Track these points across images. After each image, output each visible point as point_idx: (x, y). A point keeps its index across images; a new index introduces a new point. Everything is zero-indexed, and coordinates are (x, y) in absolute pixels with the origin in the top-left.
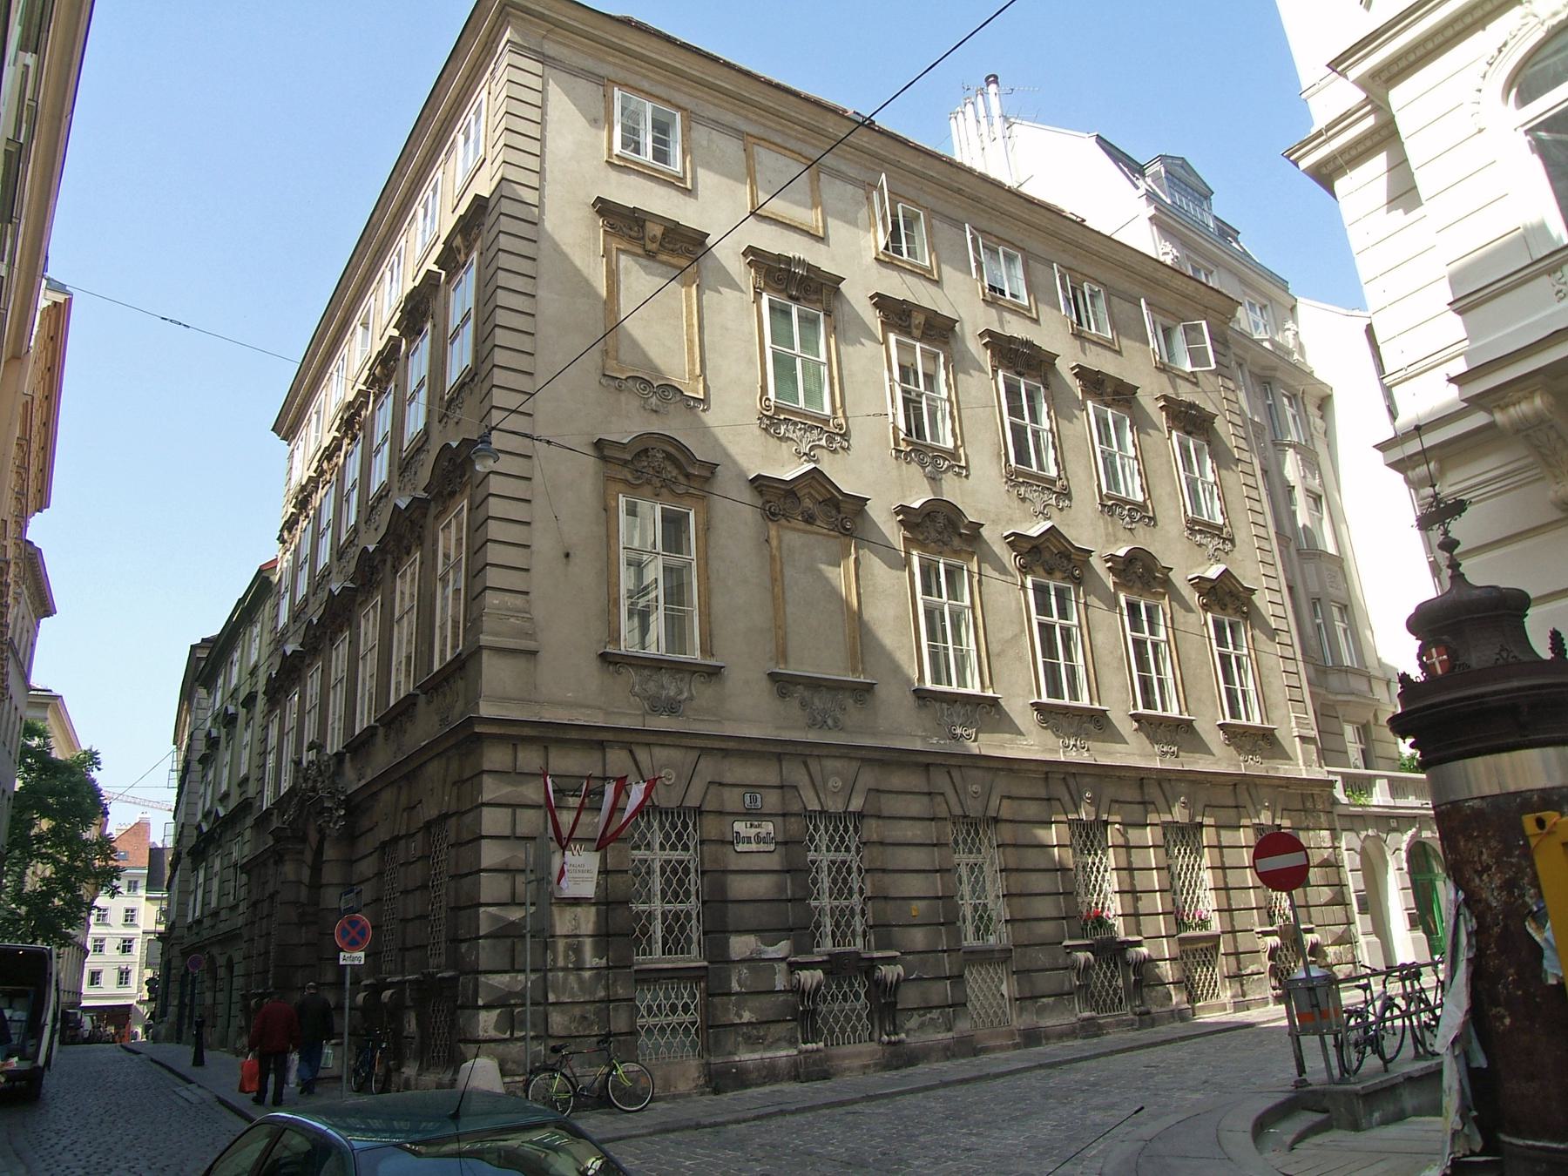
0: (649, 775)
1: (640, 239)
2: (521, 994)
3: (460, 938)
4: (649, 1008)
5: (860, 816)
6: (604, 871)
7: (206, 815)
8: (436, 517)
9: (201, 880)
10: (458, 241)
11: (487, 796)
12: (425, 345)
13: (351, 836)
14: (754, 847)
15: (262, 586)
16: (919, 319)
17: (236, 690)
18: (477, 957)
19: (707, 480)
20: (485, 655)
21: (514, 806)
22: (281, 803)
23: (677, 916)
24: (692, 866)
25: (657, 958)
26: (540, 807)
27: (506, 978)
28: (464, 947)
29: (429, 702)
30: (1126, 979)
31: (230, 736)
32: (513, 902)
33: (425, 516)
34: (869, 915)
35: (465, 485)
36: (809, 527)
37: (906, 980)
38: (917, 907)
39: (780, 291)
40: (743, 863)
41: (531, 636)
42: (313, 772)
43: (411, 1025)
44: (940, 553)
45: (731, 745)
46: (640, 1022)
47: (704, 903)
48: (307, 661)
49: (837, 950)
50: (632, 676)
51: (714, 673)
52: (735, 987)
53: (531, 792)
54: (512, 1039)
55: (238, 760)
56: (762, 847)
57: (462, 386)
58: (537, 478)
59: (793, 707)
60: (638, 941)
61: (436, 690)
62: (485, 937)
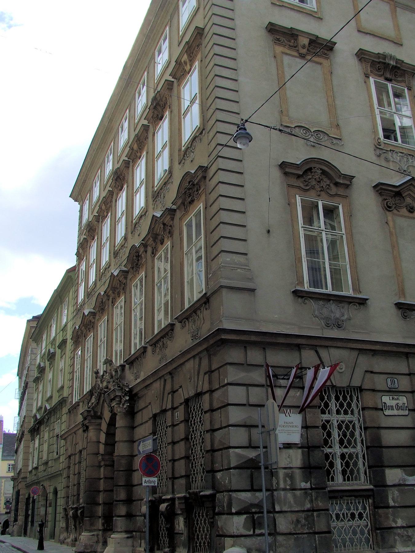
2: (259, 506)
6: (305, 427)
7: (39, 409)
8: (181, 219)
9: (37, 445)
10: (103, 207)
12: (165, 124)
14: (395, 412)
15: (70, 279)
17: (54, 339)
25: (339, 482)
26: (263, 386)
27: (249, 494)
29: (183, 327)
33: (173, 219)
35: (200, 195)
39: (380, 76)
41: (251, 280)
42: (107, 377)
43: (180, 524)
45: (377, 347)
46: (333, 525)
47: (367, 448)
50: (313, 305)
51: (363, 302)
52: (391, 503)
55: (56, 378)
56: (401, 412)
57: (194, 139)
58: (247, 186)
60: (328, 472)
61: (187, 319)
62: (234, 468)
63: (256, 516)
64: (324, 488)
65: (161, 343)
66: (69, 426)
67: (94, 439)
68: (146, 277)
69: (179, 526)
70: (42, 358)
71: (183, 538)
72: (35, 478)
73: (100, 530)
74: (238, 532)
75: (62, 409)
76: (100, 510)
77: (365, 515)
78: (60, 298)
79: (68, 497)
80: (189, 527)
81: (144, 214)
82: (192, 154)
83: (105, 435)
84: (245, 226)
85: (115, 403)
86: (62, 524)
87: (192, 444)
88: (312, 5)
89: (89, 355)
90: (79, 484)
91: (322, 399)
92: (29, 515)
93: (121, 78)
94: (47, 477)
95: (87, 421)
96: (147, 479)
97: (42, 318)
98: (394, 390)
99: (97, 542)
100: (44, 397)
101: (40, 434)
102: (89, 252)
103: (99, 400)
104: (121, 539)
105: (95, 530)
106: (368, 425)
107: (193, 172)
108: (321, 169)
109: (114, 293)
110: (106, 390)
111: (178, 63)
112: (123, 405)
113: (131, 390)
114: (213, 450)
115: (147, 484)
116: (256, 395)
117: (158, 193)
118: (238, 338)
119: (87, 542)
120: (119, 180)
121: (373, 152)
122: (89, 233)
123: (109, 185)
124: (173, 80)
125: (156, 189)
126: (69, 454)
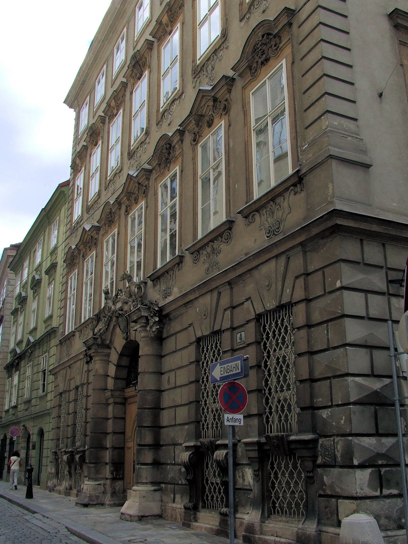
8: (103, 235)
9: (16, 381)
10: (113, 104)
15: (62, 195)
17: (40, 265)
24: (293, 403)
26: (382, 294)
29: (154, 286)
61: (257, 211)
62: (355, 403)
63: (383, 470)
65: (209, 249)
66: (60, 359)
67: (101, 372)
68: (118, 234)
69: (244, 480)
70: (24, 287)
71: (251, 496)
72: (14, 418)
73: (107, 479)
74: (362, 492)
75: (50, 341)
76: (107, 456)
78: (48, 218)
79: (59, 439)
80: (263, 482)
81: (119, 172)
82: (170, 116)
83: (115, 367)
84: (352, 84)
85: (139, 326)
86: (49, 469)
87: (266, 373)
89: (88, 278)
90: (75, 425)
92: (5, 457)
93: (100, 27)
94: (30, 417)
95: (91, 352)
96: (230, 416)
97: (22, 248)
98: (42, 413)
99: (104, 493)
100: (25, 329)
101: (20, 370)
102: (90, 162)
103: (109, 325)
104: (147, 492)
105: (102, 479)
107: (170, 134)
109: (128, 199)
110: (120, 312)
111: (159, 23)
112: (151, 327)
113: (161, 309)
114: (313, 380)
115: (231, 424)
116: (377, 307)
117: (203, 66)
118: (357, 226)
119: (92, 492)
120: (137, 66)
122: (89, 140)
123: (84, 139)
124: (153, 39)
125: (198, 62)
126: (61, 391)
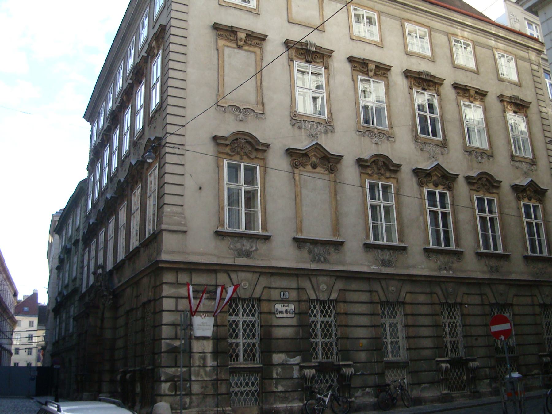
0: (235, 284)
1: (236, 40)
2: (179, 377)
3: (155, 353)
4: (237, 384)
5: (336, 301)
6: (216, 325)
8: (147, 169)
10: (154, 44)
11: (165, 293)
13: (115, 307)
14: (284, 315)
16: (372, 66)
18: (161, 362)
19: (265, 151)
20: (164, 233)
21: (177, 298)
22: (91, 289)
23: (249, 345)
25: (241, 363)
27: (173, 369)
28: (156, 356)
30: (468, 376)
31: (69, 258)
32: (176, 338)
33: (143, 168)
34: (339, 345)
36: (314, 170)
37: (355, 374)
38: (364, 342)
40: (280, 322)
41: (185, 225)
43: (138, 389)
44: (379, 179)
47: (261, 339)
48: (99, 227)
49: (324, 360)
51: (267, 238)
52: (275, 376)
53: (183, 291)
54: (176, 395)
56: (289, 315)
57: (156, 111)
59: (305, 253)
62: (165, 352)
64: (227, 366)
77: (256, 384)
88: (253, 4)
91: (231, 306)
106: (263, 324)
108: (245, 139)
121: (289, 122)
